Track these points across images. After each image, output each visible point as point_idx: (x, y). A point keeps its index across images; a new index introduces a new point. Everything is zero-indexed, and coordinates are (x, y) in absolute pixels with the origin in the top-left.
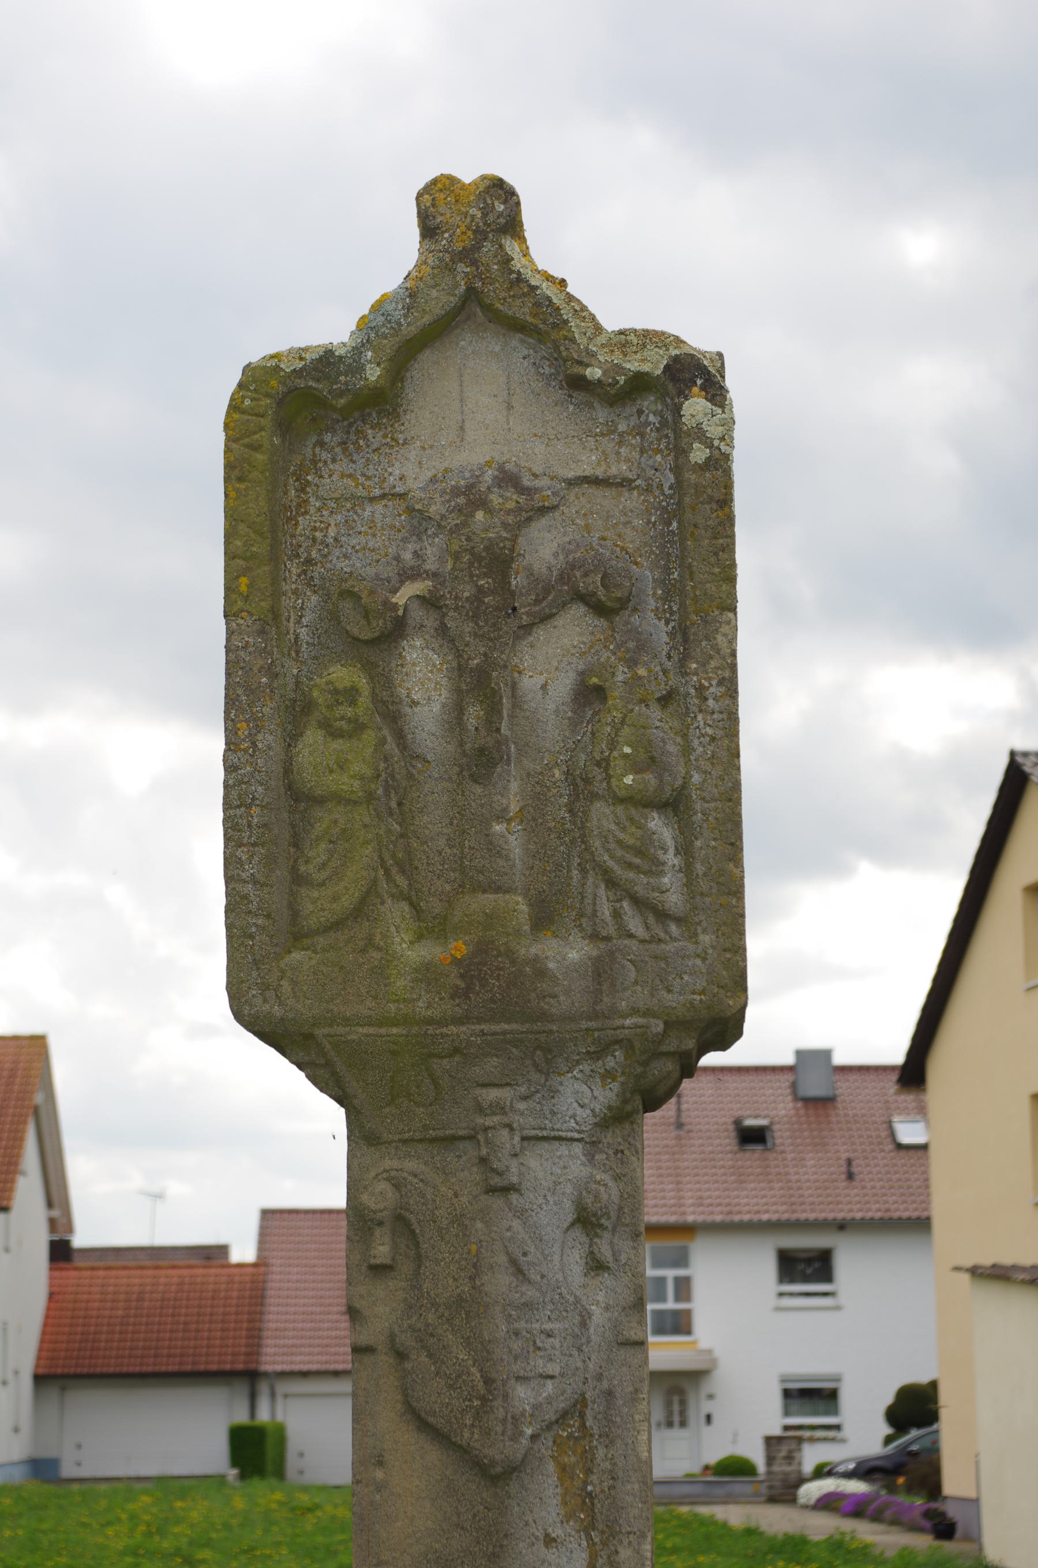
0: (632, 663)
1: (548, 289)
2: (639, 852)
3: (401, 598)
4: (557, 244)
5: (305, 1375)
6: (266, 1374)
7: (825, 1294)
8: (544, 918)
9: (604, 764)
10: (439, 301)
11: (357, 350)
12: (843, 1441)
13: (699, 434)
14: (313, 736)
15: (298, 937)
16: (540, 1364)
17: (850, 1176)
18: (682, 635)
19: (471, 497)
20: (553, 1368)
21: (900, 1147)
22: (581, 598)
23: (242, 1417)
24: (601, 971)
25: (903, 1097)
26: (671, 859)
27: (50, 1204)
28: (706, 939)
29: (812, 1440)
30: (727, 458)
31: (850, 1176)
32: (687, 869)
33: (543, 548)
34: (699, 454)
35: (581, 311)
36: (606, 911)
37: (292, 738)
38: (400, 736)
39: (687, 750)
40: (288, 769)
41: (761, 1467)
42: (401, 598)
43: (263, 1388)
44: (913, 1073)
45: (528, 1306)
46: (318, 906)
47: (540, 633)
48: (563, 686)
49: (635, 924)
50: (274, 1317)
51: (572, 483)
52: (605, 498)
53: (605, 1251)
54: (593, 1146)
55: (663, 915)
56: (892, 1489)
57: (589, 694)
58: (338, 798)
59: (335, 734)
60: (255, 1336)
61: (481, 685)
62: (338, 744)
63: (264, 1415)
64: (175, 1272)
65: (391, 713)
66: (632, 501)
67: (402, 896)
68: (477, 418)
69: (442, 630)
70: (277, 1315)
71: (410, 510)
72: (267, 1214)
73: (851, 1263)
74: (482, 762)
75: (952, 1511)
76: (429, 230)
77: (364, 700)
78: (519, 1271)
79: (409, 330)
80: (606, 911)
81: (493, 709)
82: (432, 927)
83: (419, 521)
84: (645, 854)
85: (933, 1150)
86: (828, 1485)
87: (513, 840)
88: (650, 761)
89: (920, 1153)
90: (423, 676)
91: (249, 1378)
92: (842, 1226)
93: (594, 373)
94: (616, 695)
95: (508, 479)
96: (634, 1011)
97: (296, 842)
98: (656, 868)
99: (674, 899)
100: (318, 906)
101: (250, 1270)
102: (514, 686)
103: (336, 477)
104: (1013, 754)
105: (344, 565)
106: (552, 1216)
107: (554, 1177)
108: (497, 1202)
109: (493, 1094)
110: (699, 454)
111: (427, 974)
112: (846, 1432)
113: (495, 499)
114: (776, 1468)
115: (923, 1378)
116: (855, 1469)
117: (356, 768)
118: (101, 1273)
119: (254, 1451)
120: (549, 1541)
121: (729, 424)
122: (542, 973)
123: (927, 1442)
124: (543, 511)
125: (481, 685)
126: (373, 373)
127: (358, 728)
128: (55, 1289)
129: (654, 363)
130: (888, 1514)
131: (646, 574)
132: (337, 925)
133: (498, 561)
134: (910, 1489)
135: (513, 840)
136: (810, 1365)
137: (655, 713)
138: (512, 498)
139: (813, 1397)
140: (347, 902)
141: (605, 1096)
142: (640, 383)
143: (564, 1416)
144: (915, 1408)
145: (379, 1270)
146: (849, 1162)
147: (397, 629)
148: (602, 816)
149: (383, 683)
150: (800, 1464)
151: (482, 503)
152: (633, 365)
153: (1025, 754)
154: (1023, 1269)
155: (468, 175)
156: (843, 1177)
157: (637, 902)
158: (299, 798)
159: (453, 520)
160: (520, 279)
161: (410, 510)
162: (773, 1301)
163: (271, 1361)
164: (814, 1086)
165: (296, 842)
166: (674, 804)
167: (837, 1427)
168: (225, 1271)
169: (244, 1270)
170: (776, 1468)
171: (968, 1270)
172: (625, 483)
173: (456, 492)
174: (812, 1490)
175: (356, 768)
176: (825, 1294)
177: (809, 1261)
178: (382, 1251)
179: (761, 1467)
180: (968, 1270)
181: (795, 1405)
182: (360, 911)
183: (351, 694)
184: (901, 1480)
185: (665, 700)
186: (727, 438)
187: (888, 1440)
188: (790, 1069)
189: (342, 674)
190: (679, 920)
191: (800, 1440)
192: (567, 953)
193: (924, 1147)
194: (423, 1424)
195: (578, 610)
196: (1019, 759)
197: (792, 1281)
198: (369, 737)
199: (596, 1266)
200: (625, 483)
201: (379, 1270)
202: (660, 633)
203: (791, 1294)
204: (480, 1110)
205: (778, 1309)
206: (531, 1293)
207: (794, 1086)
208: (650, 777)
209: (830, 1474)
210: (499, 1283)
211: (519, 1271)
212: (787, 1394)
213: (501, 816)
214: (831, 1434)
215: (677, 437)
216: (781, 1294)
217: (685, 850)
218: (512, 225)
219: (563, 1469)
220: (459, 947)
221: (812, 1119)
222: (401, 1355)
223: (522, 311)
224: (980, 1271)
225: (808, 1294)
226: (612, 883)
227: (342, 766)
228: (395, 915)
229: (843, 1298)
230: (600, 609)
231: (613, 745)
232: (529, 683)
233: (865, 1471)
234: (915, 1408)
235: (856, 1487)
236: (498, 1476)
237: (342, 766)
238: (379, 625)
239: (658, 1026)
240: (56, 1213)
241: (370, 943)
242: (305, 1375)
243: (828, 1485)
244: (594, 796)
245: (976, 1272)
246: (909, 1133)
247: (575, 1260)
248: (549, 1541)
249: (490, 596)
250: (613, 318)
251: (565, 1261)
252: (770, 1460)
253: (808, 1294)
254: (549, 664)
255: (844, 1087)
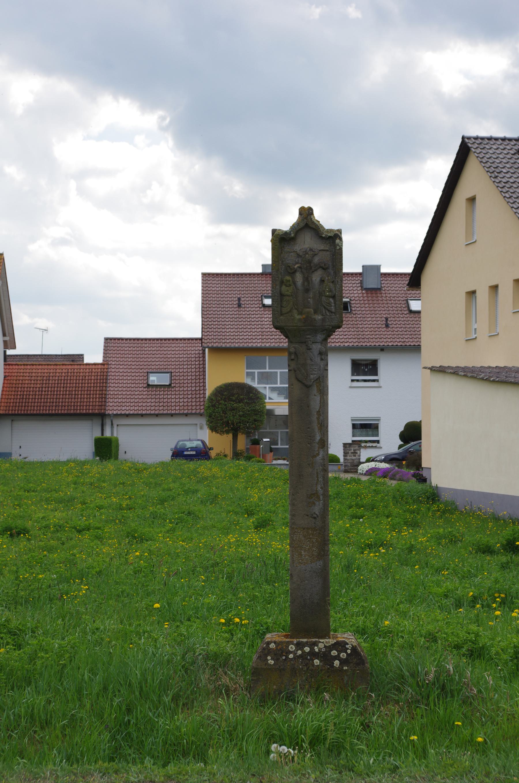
0: (328, 276)
1: (317, 223)
2: (328, 304)
3: (296, 267)
4: (317, 215)
5: (127, 416)
6: (109, 415)
7: (374, 381)
8: (315, 312)
9: (324, 291)
10: (302, 225)
11: (290, 232)
12: (381, 448)
13: (338, 245)
14: (284, 287)
15: (282, 315)
16: (314, 372)
17: (387, 326)
18: (335, 273)
19: (306, 253)
20: (316, 373)
21: (411, 312)
22: (321, 267)
23: (98, 434)
24: (323, 320)
25: (411, 292)
26: (333, 305)
27: (4, 335)
28: (338, 316)
29: (366, 447)
30: (342, 248)
31: (387, 326)
32: (335, 306)
33: (316, 260)
34: (338, 248)
35: (322, 226)
36: (324, 312)
37: (281, 286)
38: (295, 286)
39: (335, 289)
40: (280, 291)
41: (342, 460)
42: (296, 267)
43: (108, 422)
44: (415, 279)
45: (312, 365)
46: (285, 310)
47: (315, 272)
48: (318, 279)
49: (328, 314)
50: (112, 389)
51: (320, 250)
52: (324, 253)
53: (323, 357)
54: (322, 343)
55: (332, 312)
56: (400, 466)
57: (322, 281)
58: (288, 296)
59: (287, 286)
60: (103, 398)
61: (307, 280)
62: (287, 288)
63: (108, 434)
64: (64, 367)
65: (295, 283)
66: (328, 253)
67: (296, 309)
68: (307, 242)
69: (302, 271)
70: (113, 388)
71: (297, 254)
72: (107, 340)
73: (387, 367)
74: (307, 291)
75: (425, 473)
76: (300, 213)
77: (291, 282)
78: (311, 360)
79: (297, 229)
80: (324, 312)
81: (309, 283)
82: (300, 313)
83: (299, 256)
84: (329, 304)
85: (422, 314)
86: (372, 465)
87: (311, 301)
88: (330, 291)
89: (417, 315)
90: (299, 278)
91: (101, 417)
92: (382, 349)
93: (324, 236)
94: (326, 282)
95: (311, 250)
96: (328, 325)
97: (281, 301)
98: (331, 306)
99: (333, 310)
100: (285, 310)
101: (100, 367)
102: (311, 279)
103: (287, 249)
104: (463, 138)
105: (288, 262)
106: (316, 353)
107: (316, 348)
108: (309, 351)
109: (308, 336)
110: (338, 248)
111: (300, 320)
112: (381, 444)
113: (309, 253)
114: (348, 458)
115: (416, 418)
116: (384, 459)
117: (290, 291)
118: (29, 367)
119: (105, 449)
120: (315, 395)
121: (342, 244)
122: (315, 320)
123: (417, 447)
124: (316, 255)
125: (307, 280)
126: (293, 235)
127: (290, 285)
128: (7, 374)
129: (331, 234)
130: (398, 477)
131: (330, 264)
132: (287, 313)
133: (310, 262)
134: (408, 466)
135: (311, 301)
136: (365, 413)
137: (331, 284)
138: (312, 253)
139: (367, 428)
140: (289, 310)
141: (323, 337)
142: (330, 237)
143: (317, 379)
144: (412, 433)
145: (292, 360)
146: (387, 319)
147: (295, 272)
148: (324, 298)
149: (293, 278)
150: (360, 456)
151: (307, 253)
152: (329, 235)
153: (469, 138)
154: (451, 368)
155: (306, 206)
156: (384, 326)
157: (329, 311)
158: (282, 295)
159: (303, 256)
160: (313, 222)
161: (297, 254)
162: (350, 384)
163: (111, 408)
164: (371, 283)
165: (281, 301)
166: (334, 297)
167: (378, 442)
168: (82, 367)
169: (97, 367)
170: (348, 458)
171: (429, 368)
172: (327, 250)
173: (304, 252)
174: (364, 467)
175: (290, 291)
176: (374, 381)
177: (366, 365)
178: (293, 357)
179: (342, 460)
180: (429, 368)
181: (358, 431)
182: (290, 311)
183: (289, 281)
184: (404, 463)
185: (333, 282)
186: (342, 245)
187: (400, 447)
188: (360, 274)
189: (288, 278)
190: (334, 313)
191: (360, 446)
192: (319, 317)
193: (419, 312)
194: (298, 380)
195: (320, 269)
196: (466, 140)
197: (358, 375)
198: (292, 287)
199: (322, 359)
200: (327, 250)
201: (292, 360)
202: (332, 272)
203: (358, 381)
204: (306, 338)
205: (351, 387)
206: (313, 363)
207: (361, 282)
208: (330, 293)
209: (373, 460)
210: (309, 362)
211: (311, 360)
212: (354, 426)
213: (310, 298)
214: (374, 445)
215: (334, 245)
216: (353, 381)
217: (335, 303)
218: (312, 214)
219: (317, 386)
220: (304, 316)
221: (369, 295)
222: (295, 371)
223: (314, 227)
224: (434, 369)
225: (365, 381)
226: (325, 308)
227: (288, 291)
228: (295, 311)
229: (381, 383)
230: (324, 269)
231: (325, 289)
232: (314, 279)
233: (389, 459)
234: (412, 433)
235: (384, 466)
236: (308, 387)
237: (288, 291)
238: (293, 271)
239: (331, 327)
240: (7, 338)
241: (292, 316)
242: (127, 416)
243: (372, 465)
244: (322, 296)
245: (433, 369)
246: (415, 305)
247: (319, 358)
248: (315, 395)
249: (308, 267)
250: (327, 227)
251: (317, 359)
252: (345, 454)
253: (365, 381)
254: (316, 277)
255: (386, 284)
